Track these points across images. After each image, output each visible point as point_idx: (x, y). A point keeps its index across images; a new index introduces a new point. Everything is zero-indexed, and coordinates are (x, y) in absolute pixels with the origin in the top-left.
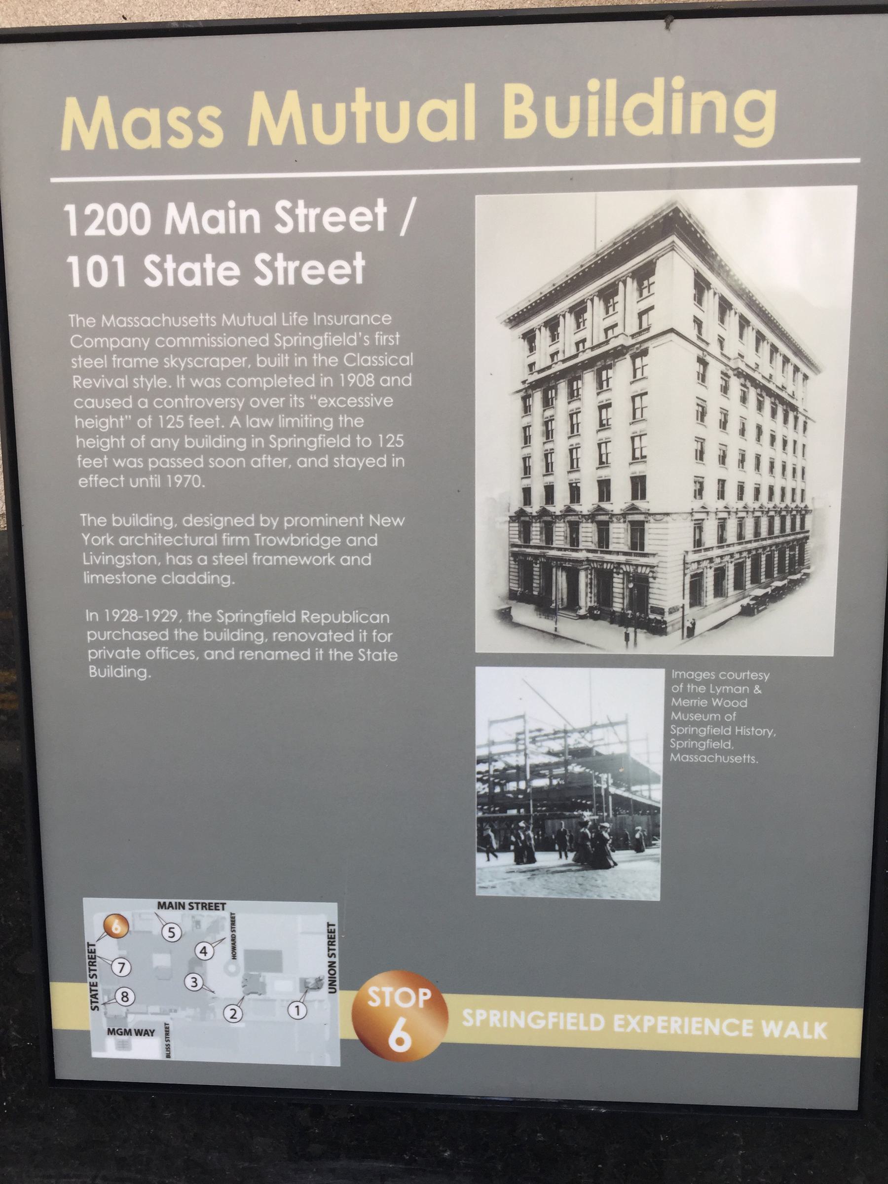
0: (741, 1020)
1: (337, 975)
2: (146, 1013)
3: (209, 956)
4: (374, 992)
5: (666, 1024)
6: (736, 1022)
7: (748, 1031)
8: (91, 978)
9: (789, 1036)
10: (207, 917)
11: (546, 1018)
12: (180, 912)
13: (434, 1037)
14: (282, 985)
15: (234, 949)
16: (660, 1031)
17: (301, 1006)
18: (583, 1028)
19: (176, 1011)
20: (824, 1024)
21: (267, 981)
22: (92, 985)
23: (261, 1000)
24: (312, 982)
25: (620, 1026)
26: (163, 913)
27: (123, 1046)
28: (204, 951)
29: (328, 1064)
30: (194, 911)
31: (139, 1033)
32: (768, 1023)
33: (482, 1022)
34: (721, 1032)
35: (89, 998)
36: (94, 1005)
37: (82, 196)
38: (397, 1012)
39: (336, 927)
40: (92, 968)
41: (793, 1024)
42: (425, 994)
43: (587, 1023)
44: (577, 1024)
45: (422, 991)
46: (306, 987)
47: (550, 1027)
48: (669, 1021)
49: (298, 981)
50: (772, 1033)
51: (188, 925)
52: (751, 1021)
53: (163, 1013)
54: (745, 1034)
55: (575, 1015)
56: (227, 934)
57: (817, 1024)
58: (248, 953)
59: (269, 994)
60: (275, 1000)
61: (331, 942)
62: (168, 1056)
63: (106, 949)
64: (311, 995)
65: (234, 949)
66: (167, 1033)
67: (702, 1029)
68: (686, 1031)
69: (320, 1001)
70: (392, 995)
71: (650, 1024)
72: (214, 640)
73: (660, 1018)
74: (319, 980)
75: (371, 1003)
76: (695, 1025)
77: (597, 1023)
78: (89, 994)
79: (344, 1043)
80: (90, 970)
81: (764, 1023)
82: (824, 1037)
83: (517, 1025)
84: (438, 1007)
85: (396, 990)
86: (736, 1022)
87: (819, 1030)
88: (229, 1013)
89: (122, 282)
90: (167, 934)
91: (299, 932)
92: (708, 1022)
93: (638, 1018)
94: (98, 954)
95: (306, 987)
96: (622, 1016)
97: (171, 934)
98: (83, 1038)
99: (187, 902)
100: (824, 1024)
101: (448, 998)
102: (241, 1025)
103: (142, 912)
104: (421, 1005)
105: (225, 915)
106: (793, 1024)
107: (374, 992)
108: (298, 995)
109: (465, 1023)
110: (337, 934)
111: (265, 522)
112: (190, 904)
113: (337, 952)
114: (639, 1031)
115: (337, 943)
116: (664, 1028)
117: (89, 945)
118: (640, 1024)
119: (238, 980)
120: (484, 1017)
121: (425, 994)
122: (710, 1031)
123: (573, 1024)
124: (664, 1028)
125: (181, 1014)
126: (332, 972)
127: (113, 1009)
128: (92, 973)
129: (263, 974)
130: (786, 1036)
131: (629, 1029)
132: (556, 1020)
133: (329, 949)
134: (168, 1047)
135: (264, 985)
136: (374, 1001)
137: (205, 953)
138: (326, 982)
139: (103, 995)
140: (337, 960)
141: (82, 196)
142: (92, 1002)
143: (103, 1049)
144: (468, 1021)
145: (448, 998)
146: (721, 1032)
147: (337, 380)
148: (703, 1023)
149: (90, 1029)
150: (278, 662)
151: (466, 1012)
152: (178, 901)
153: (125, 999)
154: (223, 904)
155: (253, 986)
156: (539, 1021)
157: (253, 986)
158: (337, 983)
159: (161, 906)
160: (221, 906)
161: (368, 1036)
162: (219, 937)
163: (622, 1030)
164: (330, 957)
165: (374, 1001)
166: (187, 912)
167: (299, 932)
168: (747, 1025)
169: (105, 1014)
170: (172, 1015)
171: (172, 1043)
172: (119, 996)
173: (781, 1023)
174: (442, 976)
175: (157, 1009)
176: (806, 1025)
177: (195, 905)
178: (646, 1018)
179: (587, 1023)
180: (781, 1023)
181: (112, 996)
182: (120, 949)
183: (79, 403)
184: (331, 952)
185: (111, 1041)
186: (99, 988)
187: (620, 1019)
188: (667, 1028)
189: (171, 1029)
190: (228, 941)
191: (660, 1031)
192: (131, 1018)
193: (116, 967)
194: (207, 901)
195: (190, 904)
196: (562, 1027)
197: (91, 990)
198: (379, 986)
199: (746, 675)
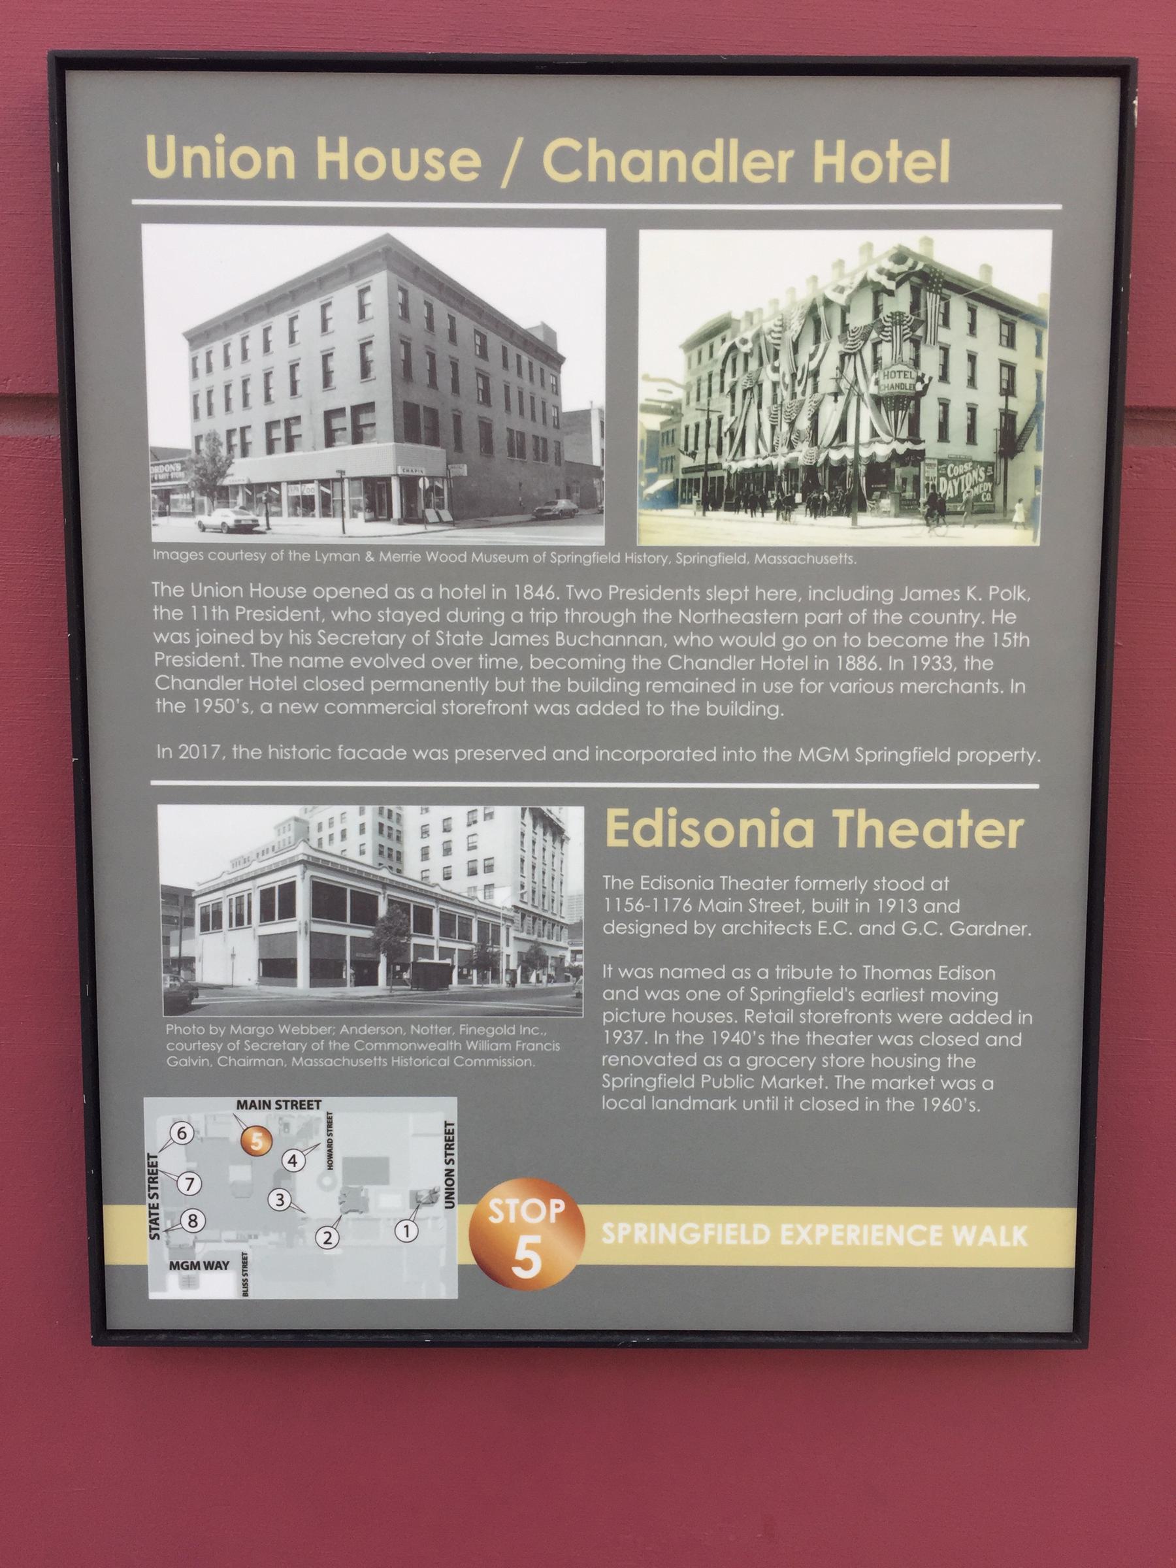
1: (456, 1186)
2: (218, 1241)
3: (299, 1166)
4: (497, 1205)
6: (923, 1228)
7: (937, 1239)
11: (701, 1231)
13: (568, 1259)
14: (389, 1201)
15: (330, 1156)
16: (835, 1242)
17: (411, 1224)
18: (744, 1241)
19: (256, 1237)
20: (1024, 1228)
21: (371, 1196)
24: (425, 1196)
25: (788, 1238)
26: (244, 1114)
27: (188, 1283)
28: (293, 1161)
30: (282, 1112)
31: (209, 1266)
35: (148, 1224)
36: (153, 1232)
39: (455, 1127)
41: (988, 1229)
42: (558, 1206)
43: (749, 1236)
44: (738, 1238)
45: (553, 1202)
47: (706, 1241)
48: (845, 1230)
52: (940, 1227)
54: (933, 1243)
56: (323, 1138)
57: (1016, 1228)
58: (346, 1161)
59: (372, 1213)
60: (379, 1219)
61: (449, 1146)
62: (245, 1294)
63: (171, 1162)
64: (424, 1211)
65: (330, 1156)
66: (245, 1264)
67: (883, 1239)
68: (865, 1243)
69: (436, 1218)
73: (835, 1227)
74: (434, 1192)
75: (492, 1219)
77: (761, 1234)
78: (148, 1219)
80: (150, 1188)
81: (955, 1228)
82: (1024, 1243)
84: (573, 1222)
85: (522, 1201)
86: (923, 1228)
87: (1018, 1234)
88: (322, 1237)
91: (411, 1134)
92: (890, 1228)
95: (418, 1202)
96: (791, 1226)
98: (139, 1273)
99: (274, 1099)
100: (1024, 1228)
101: (584, 1209)
103: (219, 1117)
104: (553, 1219)
105: (319, 1115)
106: (988, 1229)
107: (497, 1205)
108: (408, 1212)
113: (455, 1158)
114: (810, 1242)
115: (456, 1146)
116: (839, 1238)
117: (149, 1157)
118: (812, 1234)
119: (335, 1195)
121: (558, 1206)
122: (894, 1242)
124: (839, 1238)
125: (262, 1240)
126: (450, 1182)
127: (178, 1237)
129: (365, 1187)
130: (980, 1244)
131: (798, 1242)
132: (712, 1233)
133: (446, 1155)
134: (245, 1284)
135: (366, 1201)
136: (496, 1216)
137: (295, 1163)
138: (442, 1195)
140: (455, 1167)
143: (163, 1288)
144: (609, 1238)
145: (584, 1209)
148: (884, 1230)
151: (606, 1227)
152: (262, 1099)
153: (193, 1224)
154: (318, 1102)
155: (353, 1203)
156: (692, 1235)
157: (353, 1203)
158: (456, 1196)
159: (241, 1105)
160: (315, 1104)
161: (489, 1262)
162: (312, 1143)
163: (790, 1242)
165: (496, 1216)
166: (273, 1112)
167: (411, 1134)
168: (935, 1232)
169: (168, 1243)
170: (252, 1242)
174: (577, 1182)
175: (231, 1235)
176: (1003, 1229)
177: (283, 1104)
179: (749, 1236)
180: (974, 1229)
182: (188, 1160)
184: (449, 1158)
185: (174, 1277)
186: (161, 1211)
187: (788, 1230)
188: (844, 1239)
190: (323, 1148)
191: (835, 1242)
192: (199, 1247)
193: (183, 1184)
194: (298, 1099)
196: (720, 1241)
197: (150, 1214)
198: (503, 1198)
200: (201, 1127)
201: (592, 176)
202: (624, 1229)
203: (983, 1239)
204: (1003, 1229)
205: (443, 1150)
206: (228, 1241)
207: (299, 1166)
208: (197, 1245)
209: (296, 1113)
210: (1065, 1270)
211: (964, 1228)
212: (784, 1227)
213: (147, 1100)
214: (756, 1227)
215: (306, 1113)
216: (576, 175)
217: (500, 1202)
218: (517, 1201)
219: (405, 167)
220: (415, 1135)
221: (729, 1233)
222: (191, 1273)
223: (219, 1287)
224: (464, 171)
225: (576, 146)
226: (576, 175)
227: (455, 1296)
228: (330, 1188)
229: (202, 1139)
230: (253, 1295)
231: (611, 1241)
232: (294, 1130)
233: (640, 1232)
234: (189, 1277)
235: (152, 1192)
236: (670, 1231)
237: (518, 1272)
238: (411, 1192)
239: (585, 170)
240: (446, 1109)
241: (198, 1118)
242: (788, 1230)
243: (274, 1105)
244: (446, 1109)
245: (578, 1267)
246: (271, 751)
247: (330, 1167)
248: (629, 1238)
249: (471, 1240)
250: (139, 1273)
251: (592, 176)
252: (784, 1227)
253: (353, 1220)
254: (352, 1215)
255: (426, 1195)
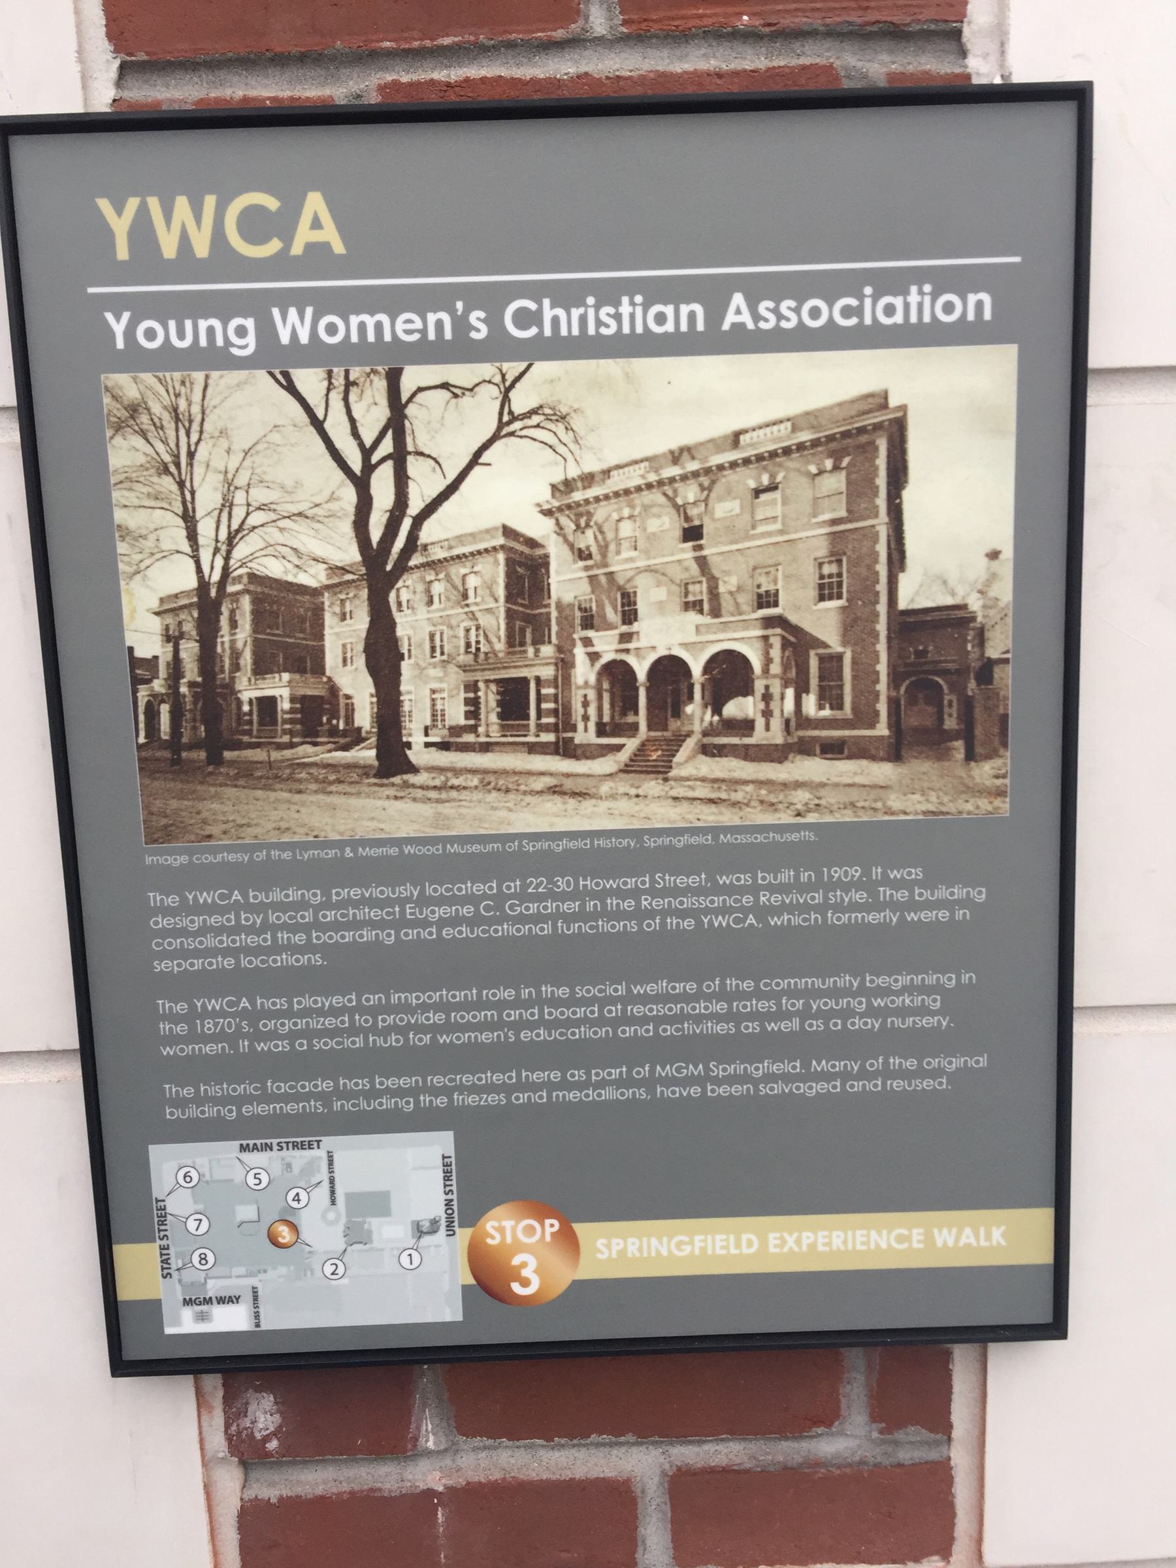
0: (910, 1230)
1: (456, 1215)
2: (230, 1277)
3: (303, 1204)
4: (493, 1227)
5: (827, 1240)
6: (905, 1232)
7: (919, 1242)
8: (161, 1239)
9: (965, 1244)
10: (299, 1158)
11: (691, 1243)
12: (268, 1154)
13: (564, 1276)
14: (390, 1232)
15: (333, 1192)
16: (821, 1248)
17: (415, 1255)
18: (733, 1251)
19: (265, 1271)
20: (1003, 1228)
21: (374, 1228)
22: (162, 1248)
23: (367, 1251)
24: (426, 1225)
25: (776, 1246)
26: (248, 1157)
27: (202, 1317)
28: (297, 1198)
29: (448, 1319)
30: (284, 1153)
31: (221, 1300)
32: (940, 1232)
33: (619, 1252)
34: (889, 1245)
35: (160, 1264)
36: (165, 1272)
37: (117, 304)
38: (519, 1248)
39: (453, 1160)
40: (162, 1228)
41: (968, 1231)
42: (552, 1225)
43: (738, 1245)
44: (727, 1248)
45: (548, 1222)
46: (419, 1231)
47: (697, 1252)
48: (830, 1237)
49: (409, 1227)
50: (945, 1244)
51: (277, 1169)
52: (921, 1231)
53: (250, 1275)
54: (916, 1245)
55: (724, 1237)
56: (324, 1175)
57: (994, 1229)
58: (350, 1197)
59: (376, 1244)
60: (383, 1250)
61: (447, 1178)
62: (258, 1325)
63: (179, 1204)
64: (427, 1240)
65: (333, 1192)
66: (256, 1298)
67: (867, 1243)
68: (850, 1247)
69: (437, 1246)
70: (514, 1229)
71: (809, 1241)
72: (262, 901)
73: (820, 1234)
74: (435, 1222)
75: (489, 1241)
76: (859, 1239)
77: (750, 1243)
78: (159, 1259)
79: (465, 1289)
80: (160, 1231)
81: (936, 1231)
82: (1003, 1243)
83: (658, 1252)
84: (568, 1240)
85: (518, 1223)
86: (905, 1232)
87: (997, 1235)
88: (329, 1269)
89: (167, 1051)
90: (251, 1181)
91: (411, 1169)
92: (874, 1234)
93: (795, 1235)
94: (168, 1210)
95: (419, 1231)
96: (778, 1235)
97: (257, 1181)
98: (153, 1308)
99: (275, 1141)
100: (1003, 1228)
101: (579, 1228)
102: (345, 1281)
103: (219, 1159)
104: (548, 1238)
105: (320, 1154)
106: (968, 1231)
107: (493, 1227)
108: (411, 1242)
109: (599, 1256)
110: (454, 1167)
111: (247, 919)
112: (278, 1144)
113: (454, 1188)
114: (796, 1249)
115: (454, 1178)
116: (825, 1245)
117: (157, 1201)
118: (798, 1242)
119: (340, 1229)
120: (621, 1247)
121: (552, 1225)
122: (877, 1245)
123: (722, 1248)
124: (825, 1245)
125: (271, 1274)
126: (450, 1212)
127: (189, 1275)
128: (162, 1234)
129: (368, 1220)
130: (961, 1244)
131: (786, 1250)
132: (703, 1244)
133: (445, 1186)
134: (257, 1316)
135: (370, 1232)
136: (493, 1238)
137: (299, 1200)
138: (443, 1223)
139: (177, 1258)
140: (454, 1197)
141: (117, 304)
142: (163, 1269)
143: (177, 1322)
144: (603, 1253)
145: (579, 1228)
146: (889, 1245)
147: (192, 1027)
148: (868, 1236)
149: (162, 1297)
150: (190, 1058)
151: (600, 1243)
152: (264, 1141)
153: (203, 1262)
154: (318, 1142)
155: (356, 1235)
156: (683, 1247)
157: (356, 1235)
158: (456, 1224)
159: (243, 1148)
160: (315, 1144)
161: (488, 1280)
162: (314, 1181)
163: (777, 1250)
164: (447, 1194)
165: (493, 1238)
166: (275, 1153)
167: (411, 1169)
168: (917, 1234)
169: (180, 1281)
170: (262, 1276)
171: (261, 1310)
172: (196, 1259)
173: (954, 1230)
174: (569, 1204)
175: (242, 1270)
176: (982, 1230)
177: (284, 1145)
178: (805, 1234)
179: (738, 1245)
180: (954, 1230)
181: (187, 1260)
182: (195, 1203)
183: (158, 944)
184: (448, 1189)
185: (187, 1314)
186: (172, 1251)
187: (775, 1238)
188: (829, 1244)
189: (260, 1293)
190: (326, 1185)
191: (821, 1248)
192: (211, 1283)
193: (192, 1225)
194: (299, 1140)
195: (278, 1144)
196: (710, 1252)
197: (162, 1255)
198: (499, 1220)
199: (441, 996)
200: (205, 1171)
201: (548, 332)
202: (617, 1244)
203: (963, 1241)
204: (982, 1230)
205: (442, 1182)
206: (238, 1277)
207: (303, 1204)
208: (209, 1281)
209: (298, 1153)
210: (1049, 1265)
211: (945, 1231)
212: (771, 1236)
213: (151, 1147)
214: (744, 1237)
215: (307, 1153)
216: (533, 331)
217: (496, 1224)
218: (512, 1223)
219: (181, 336)
220: (415, 1169)
221: (719, 1244)
222: (204, 1308)
223: (231, 1320)
224: (408, 332)
225: (533, 306)
226: (533, 331)
227: (459, 1317)
228: (336, 1221)
229: (207, 1182)
230: (264, 1326)
231: (605, 1256)
232: (296, 1169)
233: (633, 1247)
234: (202, 1312)
235: (162, 1234)
236: (661, 1243)
237: (516, 1288)
238: (413, 1222)
239: (540, 325)
240: (442, 1143)
241: (202, 1162)
242: (775, 1238)
243: (275, 1147)
244: (442, 1143)
245: (574, 1282)
246: (659, 1090)
247: (333, 1202)
248: (622, 1253)
249: (470, 1261)
250: (153, 1308)
251: (548, 332)
252: (771, 1236)
253: (359, 1251)
254: (356, 1246)
255: (427, 1224)
